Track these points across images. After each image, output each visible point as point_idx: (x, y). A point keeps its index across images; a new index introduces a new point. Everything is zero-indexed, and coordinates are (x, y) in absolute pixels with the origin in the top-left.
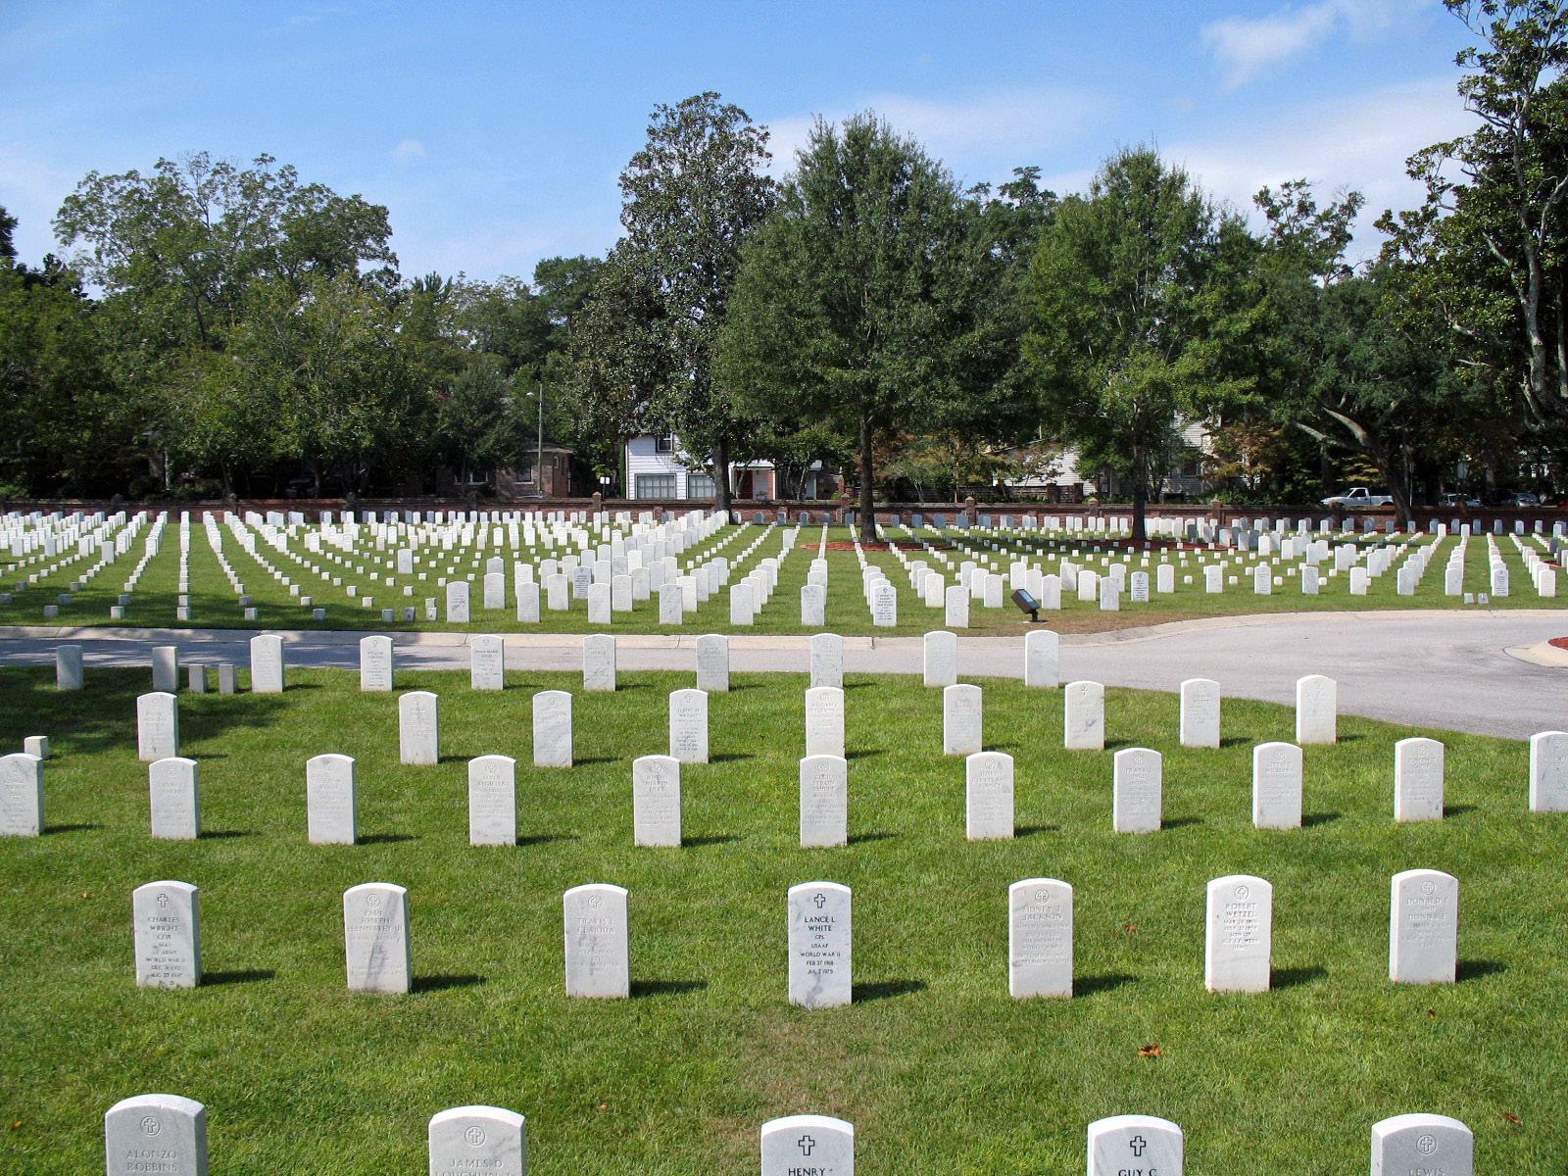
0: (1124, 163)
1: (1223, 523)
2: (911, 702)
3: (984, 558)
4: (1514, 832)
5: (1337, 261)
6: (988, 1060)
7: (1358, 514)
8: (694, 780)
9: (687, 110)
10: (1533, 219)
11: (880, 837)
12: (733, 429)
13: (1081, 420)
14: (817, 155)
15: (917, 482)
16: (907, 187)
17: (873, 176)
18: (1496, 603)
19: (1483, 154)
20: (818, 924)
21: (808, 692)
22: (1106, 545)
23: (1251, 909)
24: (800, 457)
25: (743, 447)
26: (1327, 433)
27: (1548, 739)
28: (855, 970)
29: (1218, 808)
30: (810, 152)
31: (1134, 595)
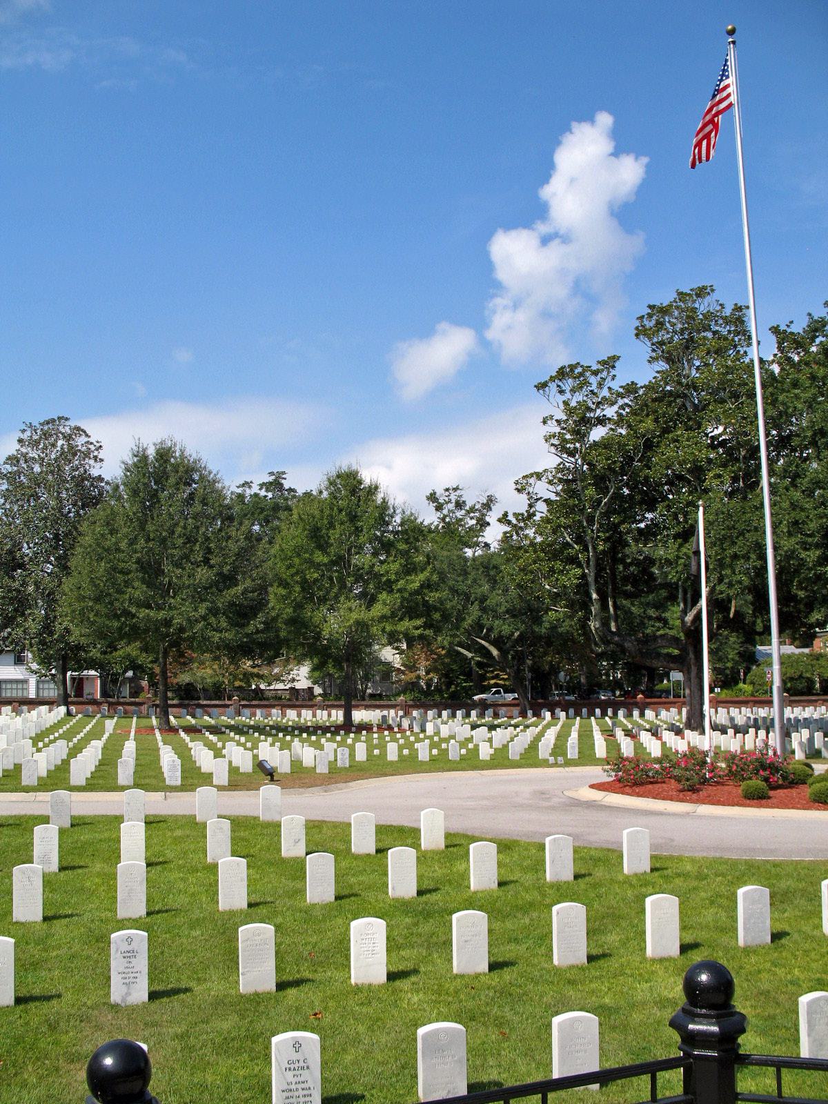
0: (338, 476)
1: (407, 714)
2: (188, 832)
3: (243, 739)
4: (536, 893)
5: (480, 539)
6: (226, 1026)
7: (495, 705)
8: (49, 882)
9: (46, 428)
10: (591, 520)
11: (167, 911)
12: (71, 649)
13: (310, 646)
14: (135, 465)
15: (199, 686)
16: (195, 489)
17: (172, 480)
18: (569, 763)
19: (560, 480)
20: (129, 954)
21: (122, 825)
22: (325, 730)
23: (375, 936)
24: (117, 669)
25: (78, 662)
26: (475, 652)
27: (555, 839)
28: (150, 984)
29: (369, 888)
30: (130, 462)
31: (339, 764)
